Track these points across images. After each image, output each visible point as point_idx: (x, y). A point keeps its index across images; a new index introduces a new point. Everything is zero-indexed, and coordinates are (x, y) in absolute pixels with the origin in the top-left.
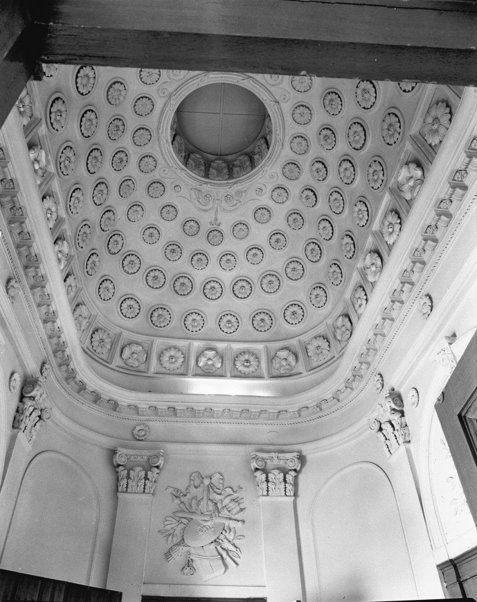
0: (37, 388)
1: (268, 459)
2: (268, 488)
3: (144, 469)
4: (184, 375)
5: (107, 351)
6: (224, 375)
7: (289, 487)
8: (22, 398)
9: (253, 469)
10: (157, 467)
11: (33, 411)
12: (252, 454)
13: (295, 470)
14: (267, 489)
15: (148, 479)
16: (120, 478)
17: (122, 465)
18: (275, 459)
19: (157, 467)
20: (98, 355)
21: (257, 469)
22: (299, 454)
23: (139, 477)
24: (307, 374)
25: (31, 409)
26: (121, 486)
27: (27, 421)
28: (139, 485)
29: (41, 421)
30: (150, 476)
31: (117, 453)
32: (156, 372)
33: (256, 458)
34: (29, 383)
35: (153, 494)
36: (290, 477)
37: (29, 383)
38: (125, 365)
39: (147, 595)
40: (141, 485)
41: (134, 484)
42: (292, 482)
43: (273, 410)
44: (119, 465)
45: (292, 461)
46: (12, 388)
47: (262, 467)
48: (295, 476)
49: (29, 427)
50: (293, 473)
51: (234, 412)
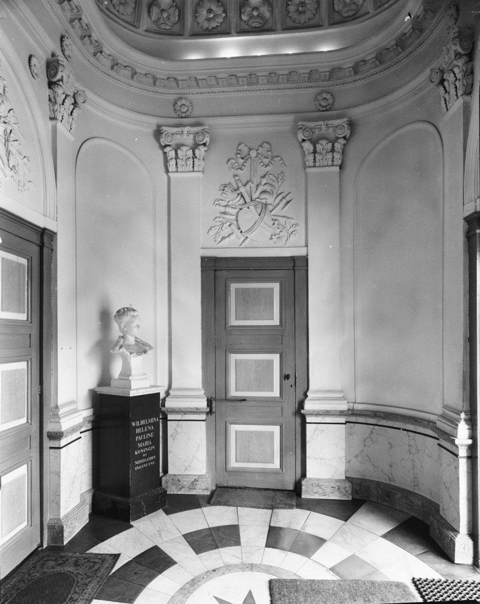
0: (61, 68)
1: (316, 129)
2: (333, 159)
3: (192, 149)
4: (180, 35)
5: (132, 11)
6: (274, 28)
7: (337, 156)
8: (51, 85)
9: (300, 140)
10: (204, 144)
11: (66, 98)
12: (299, 124)
13: (344, 138)
14: (332, 160)
15: (196, 157)
16: (169, 158)
17: (169, 145)
18: (323, 127)
19: (204, 144)
20: (122, 17)
21: (304, 140)
22: (349, 120)
23: (187, 156)
24: (144, 33)
25: (63, 97)
26: (171, 166)
27: (62, 110)
28: (188, 164)
29: (77, 109)
30: (197, 155)
31: (162, 133)
32: (192, 33)
33: (304, 129)
34: (52, 66)
35: (203, 172)
36: (338, 146)
37: (52, 66)
38: (158, 29)
39: (264, 256)
40: (173, 165)
41: (184, 163)
42: (341, 151)
43: (348, 64)
44: (166, 146)
45: (341, 129)
46: (35, 76)
47: (310, 138)
48: (344, 144)
49: (66, 116)
50: (342, 141)
51: (260, 78)
